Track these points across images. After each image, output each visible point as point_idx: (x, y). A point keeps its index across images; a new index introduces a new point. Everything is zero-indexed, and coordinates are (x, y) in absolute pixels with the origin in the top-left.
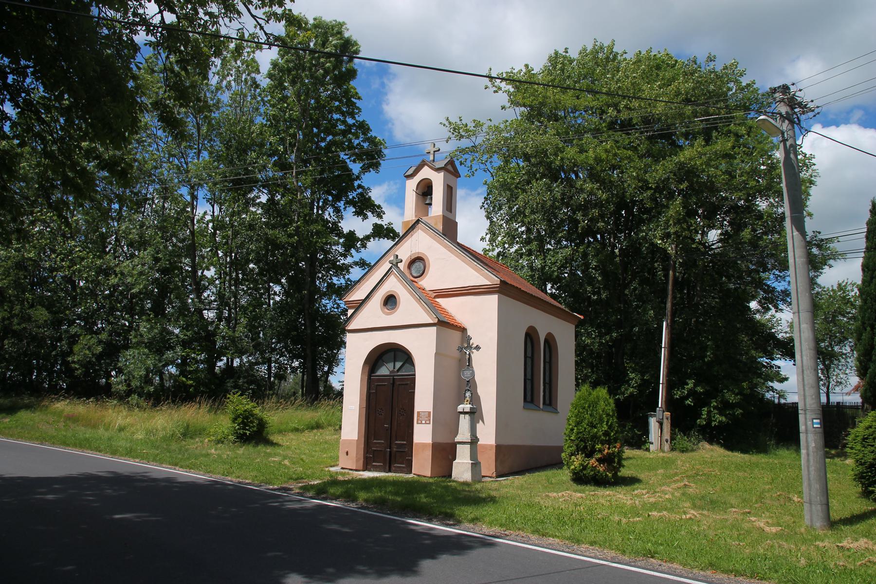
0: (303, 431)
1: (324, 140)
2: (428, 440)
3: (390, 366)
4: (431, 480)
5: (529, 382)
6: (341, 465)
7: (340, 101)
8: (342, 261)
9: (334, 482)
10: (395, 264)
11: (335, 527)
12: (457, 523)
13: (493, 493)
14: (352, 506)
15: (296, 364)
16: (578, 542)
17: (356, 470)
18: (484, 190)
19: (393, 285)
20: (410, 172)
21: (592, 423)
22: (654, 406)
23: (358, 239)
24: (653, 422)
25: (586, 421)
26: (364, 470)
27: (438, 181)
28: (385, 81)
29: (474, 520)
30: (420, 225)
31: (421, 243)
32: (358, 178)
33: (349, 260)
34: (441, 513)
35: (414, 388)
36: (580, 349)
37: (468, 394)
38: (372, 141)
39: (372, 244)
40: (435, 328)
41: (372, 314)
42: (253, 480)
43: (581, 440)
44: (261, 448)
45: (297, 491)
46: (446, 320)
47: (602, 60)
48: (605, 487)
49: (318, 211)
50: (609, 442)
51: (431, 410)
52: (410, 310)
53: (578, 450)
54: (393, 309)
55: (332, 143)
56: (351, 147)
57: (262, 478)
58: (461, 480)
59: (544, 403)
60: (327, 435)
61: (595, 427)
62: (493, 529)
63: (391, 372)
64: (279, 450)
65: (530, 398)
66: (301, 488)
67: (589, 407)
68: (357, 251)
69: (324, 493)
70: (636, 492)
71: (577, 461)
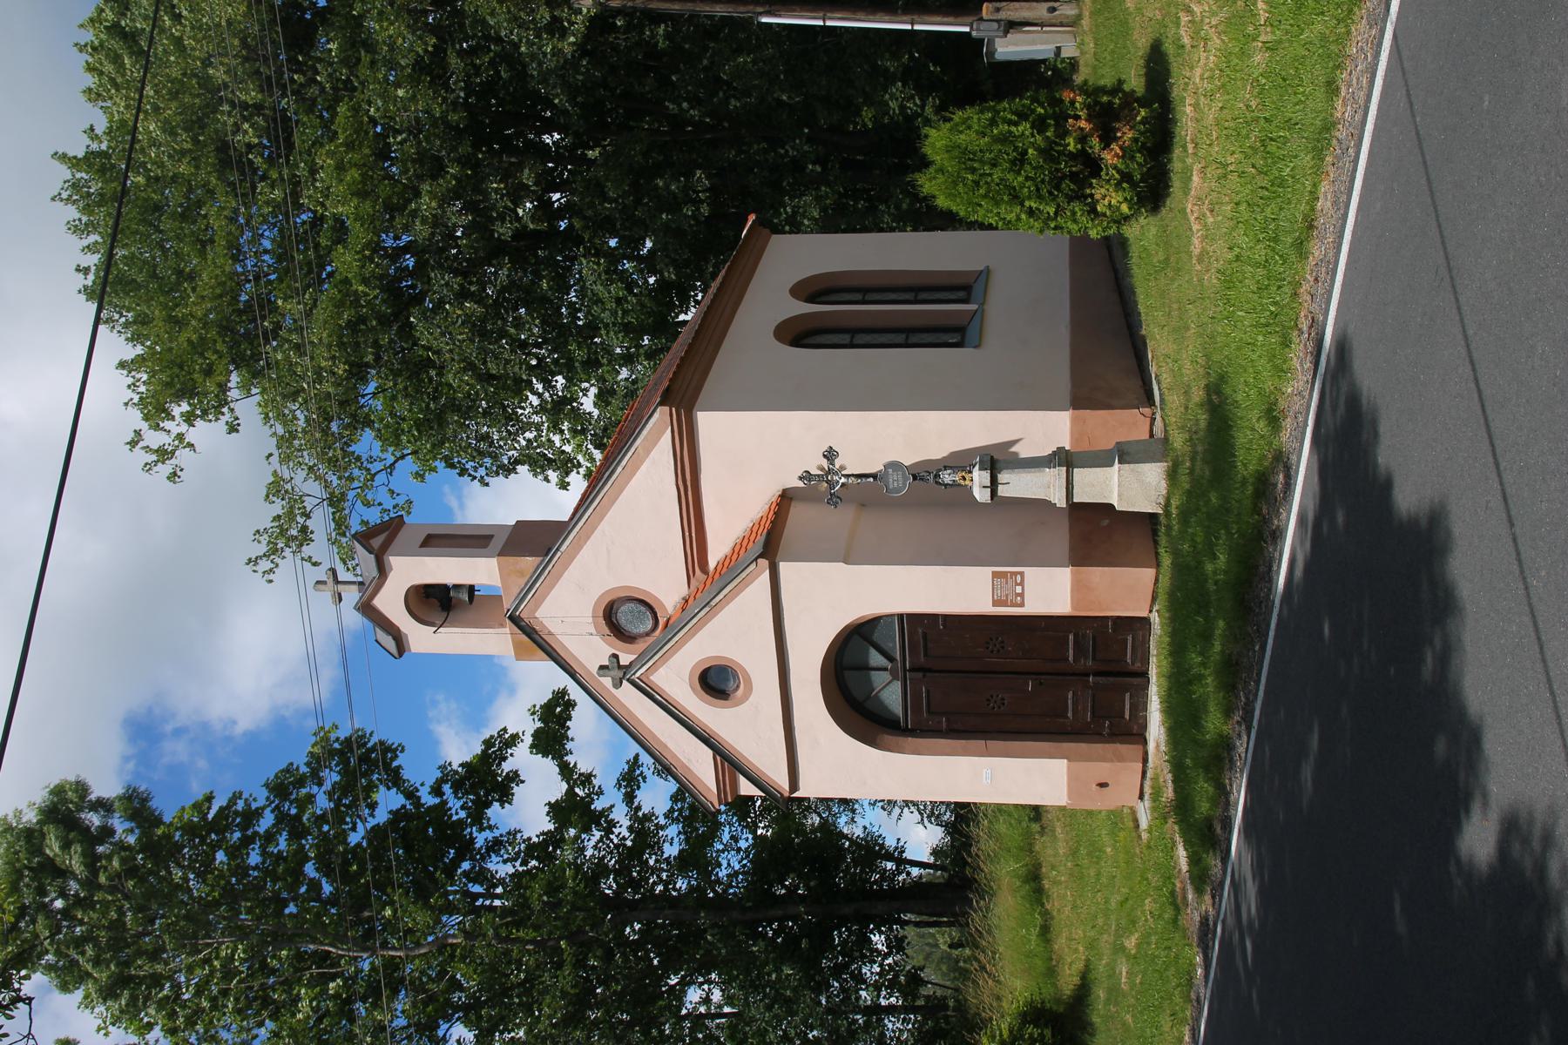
0: (1046, 915)
1: (315, 886)
2: (1062, 577)
3: (879, 679)
4: (1166, 560)
5: (914, 339)
6: (1132, 799)
7: (215, 847)
8: (623, 829)
9: (1182, 807)
10: (620, 672)
11: (1307, 773)
12: (1283, 462)
13: (1198, 395)
14: (1244, 747)
15: (878, 940)
16: (1329, 126)
17: (1145, 760)
18: (443, 475)
19: (675, 675)
20: (389, 642)
21: (1013, 162)
22: (969, 47)
23: (570, 792)
24: (1009, 48)
25: (1010, 177)
26: (1145, 742)
27: (413, 569)
28: (169, 728)
29: (1273, 418)
30: (524, 613)
31: (569, 608)
32: (411, 795)
33: (621, 815)
34: (1256, 510)
35: (933, 617)
36: (832, 223)
37: (947, 477)
38: (317, 764)
39: (583, 758)
40: (783, 567)
41: (749, 726)
42: (1183, 1021)
43: (1058, 188)
44: (1099, 1011)
45: (1207, 898)
46: (761, 539)
47: (114, 193)
48: (1174, 121)
49: (498, 897)
50: (1061, 118)
51: (988, 570)
52: (736, 631)
53: (1079, 196)
54: (735, 675)
55: (325, 868)
56: (338, 816)
57: (1177, 999)
58: (1163, 484)
59: (966, 301)
60: (1055, 851)
61: (1025, 153)
62: (1296, 363)
63: (895, 678)
64: (1101, 967)
65: (955, 334)
66: (1199, 891)
67: (973, 171)
68: (600, 793)
69: (1210, 827)
70: (1186, 40)
71: (1110, 197)
